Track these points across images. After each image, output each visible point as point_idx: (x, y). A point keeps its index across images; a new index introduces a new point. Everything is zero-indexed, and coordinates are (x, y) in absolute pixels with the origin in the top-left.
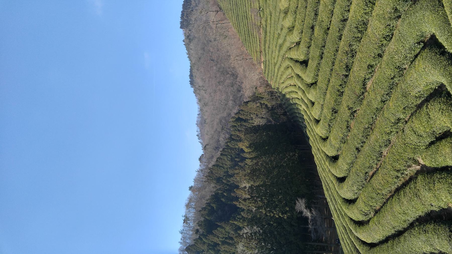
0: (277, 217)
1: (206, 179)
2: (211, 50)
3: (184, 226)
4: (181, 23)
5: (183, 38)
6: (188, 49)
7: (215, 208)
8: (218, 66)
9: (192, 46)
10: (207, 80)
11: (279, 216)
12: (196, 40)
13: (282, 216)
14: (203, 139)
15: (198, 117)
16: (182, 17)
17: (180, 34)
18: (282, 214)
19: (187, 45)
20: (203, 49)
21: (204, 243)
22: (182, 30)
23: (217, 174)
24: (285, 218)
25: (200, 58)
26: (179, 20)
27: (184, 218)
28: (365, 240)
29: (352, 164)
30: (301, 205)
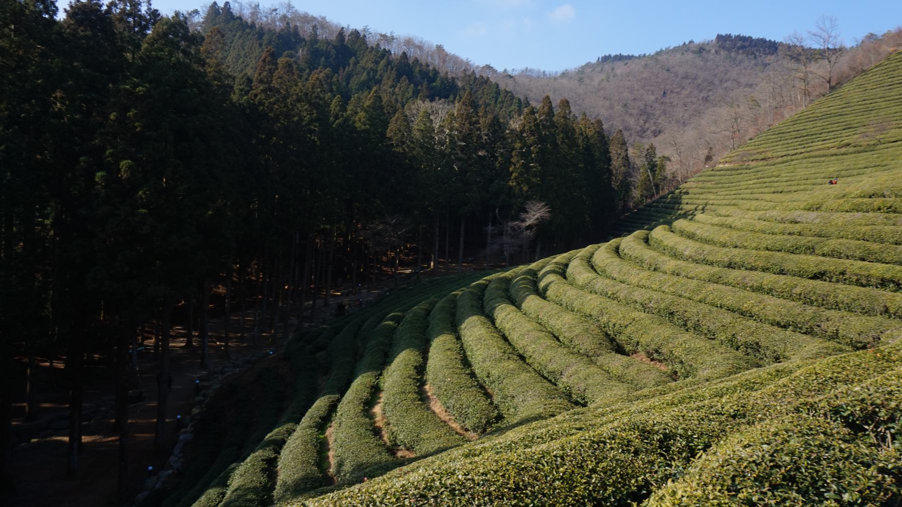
0: (511, 169)
1: (468, 73)
2: (685, 92)
3: (376, 34)
4: (729, 37)
5: (698, 40)
6: (676, 49)
7: (434, 84)
8: (657, 105)
9: (689, 56)
10: (628, 83)
11: (512, 172)
12: (702, 63)
13: (512, 177)
14: (520, 76)
15: (539, 71)
16: (740, 38)
17: (705, 34)
18: (516, 178)
19: (685, 48)
20: (686, 77)
21: (377, 63)
22: (715, 36)
23: (480, 92)
24: (510, 183)
25: (668, 70)
26: (734, 33)
27: (389, 35)
28: (430, 376)
29: (764, 232)
30: (535, 213)
